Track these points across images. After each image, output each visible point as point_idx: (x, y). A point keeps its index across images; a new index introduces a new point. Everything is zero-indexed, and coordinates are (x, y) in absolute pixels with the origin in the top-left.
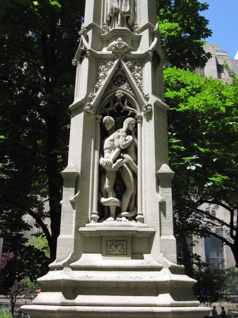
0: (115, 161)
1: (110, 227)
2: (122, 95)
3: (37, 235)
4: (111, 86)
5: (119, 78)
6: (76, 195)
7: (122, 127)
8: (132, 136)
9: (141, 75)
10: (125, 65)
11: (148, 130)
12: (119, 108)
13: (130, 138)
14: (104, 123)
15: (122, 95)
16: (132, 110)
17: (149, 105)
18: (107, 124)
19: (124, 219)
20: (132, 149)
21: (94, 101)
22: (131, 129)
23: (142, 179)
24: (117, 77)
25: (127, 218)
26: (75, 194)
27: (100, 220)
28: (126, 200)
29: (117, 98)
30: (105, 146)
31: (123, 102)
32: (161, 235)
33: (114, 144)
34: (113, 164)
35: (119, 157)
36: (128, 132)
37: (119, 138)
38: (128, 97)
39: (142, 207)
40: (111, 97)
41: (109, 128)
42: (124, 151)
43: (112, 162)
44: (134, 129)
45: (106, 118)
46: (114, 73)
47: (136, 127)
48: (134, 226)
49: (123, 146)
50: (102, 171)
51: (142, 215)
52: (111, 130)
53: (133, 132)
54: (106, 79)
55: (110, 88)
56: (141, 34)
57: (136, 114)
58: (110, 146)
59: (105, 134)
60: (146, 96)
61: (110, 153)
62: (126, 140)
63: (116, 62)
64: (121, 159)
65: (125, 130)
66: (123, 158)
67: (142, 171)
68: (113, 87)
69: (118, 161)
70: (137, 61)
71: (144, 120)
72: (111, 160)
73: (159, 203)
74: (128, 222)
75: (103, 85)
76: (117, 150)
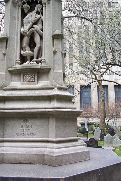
19: (35, 62)
22: (39, 10)
25: (37, 62)
35: (32, 27)
36: (38, 13)
37: (31, 17)
43: (27, 31)
44: (41, 11)
47: (42, 9)
49: (34, 21)
50: (22, 36)
51: (45, 59)
53: (40, 12)
59: (24, 15)
61: (27, 25)
66: (34, 28)
73: (53, 52)
76: (31, 23)
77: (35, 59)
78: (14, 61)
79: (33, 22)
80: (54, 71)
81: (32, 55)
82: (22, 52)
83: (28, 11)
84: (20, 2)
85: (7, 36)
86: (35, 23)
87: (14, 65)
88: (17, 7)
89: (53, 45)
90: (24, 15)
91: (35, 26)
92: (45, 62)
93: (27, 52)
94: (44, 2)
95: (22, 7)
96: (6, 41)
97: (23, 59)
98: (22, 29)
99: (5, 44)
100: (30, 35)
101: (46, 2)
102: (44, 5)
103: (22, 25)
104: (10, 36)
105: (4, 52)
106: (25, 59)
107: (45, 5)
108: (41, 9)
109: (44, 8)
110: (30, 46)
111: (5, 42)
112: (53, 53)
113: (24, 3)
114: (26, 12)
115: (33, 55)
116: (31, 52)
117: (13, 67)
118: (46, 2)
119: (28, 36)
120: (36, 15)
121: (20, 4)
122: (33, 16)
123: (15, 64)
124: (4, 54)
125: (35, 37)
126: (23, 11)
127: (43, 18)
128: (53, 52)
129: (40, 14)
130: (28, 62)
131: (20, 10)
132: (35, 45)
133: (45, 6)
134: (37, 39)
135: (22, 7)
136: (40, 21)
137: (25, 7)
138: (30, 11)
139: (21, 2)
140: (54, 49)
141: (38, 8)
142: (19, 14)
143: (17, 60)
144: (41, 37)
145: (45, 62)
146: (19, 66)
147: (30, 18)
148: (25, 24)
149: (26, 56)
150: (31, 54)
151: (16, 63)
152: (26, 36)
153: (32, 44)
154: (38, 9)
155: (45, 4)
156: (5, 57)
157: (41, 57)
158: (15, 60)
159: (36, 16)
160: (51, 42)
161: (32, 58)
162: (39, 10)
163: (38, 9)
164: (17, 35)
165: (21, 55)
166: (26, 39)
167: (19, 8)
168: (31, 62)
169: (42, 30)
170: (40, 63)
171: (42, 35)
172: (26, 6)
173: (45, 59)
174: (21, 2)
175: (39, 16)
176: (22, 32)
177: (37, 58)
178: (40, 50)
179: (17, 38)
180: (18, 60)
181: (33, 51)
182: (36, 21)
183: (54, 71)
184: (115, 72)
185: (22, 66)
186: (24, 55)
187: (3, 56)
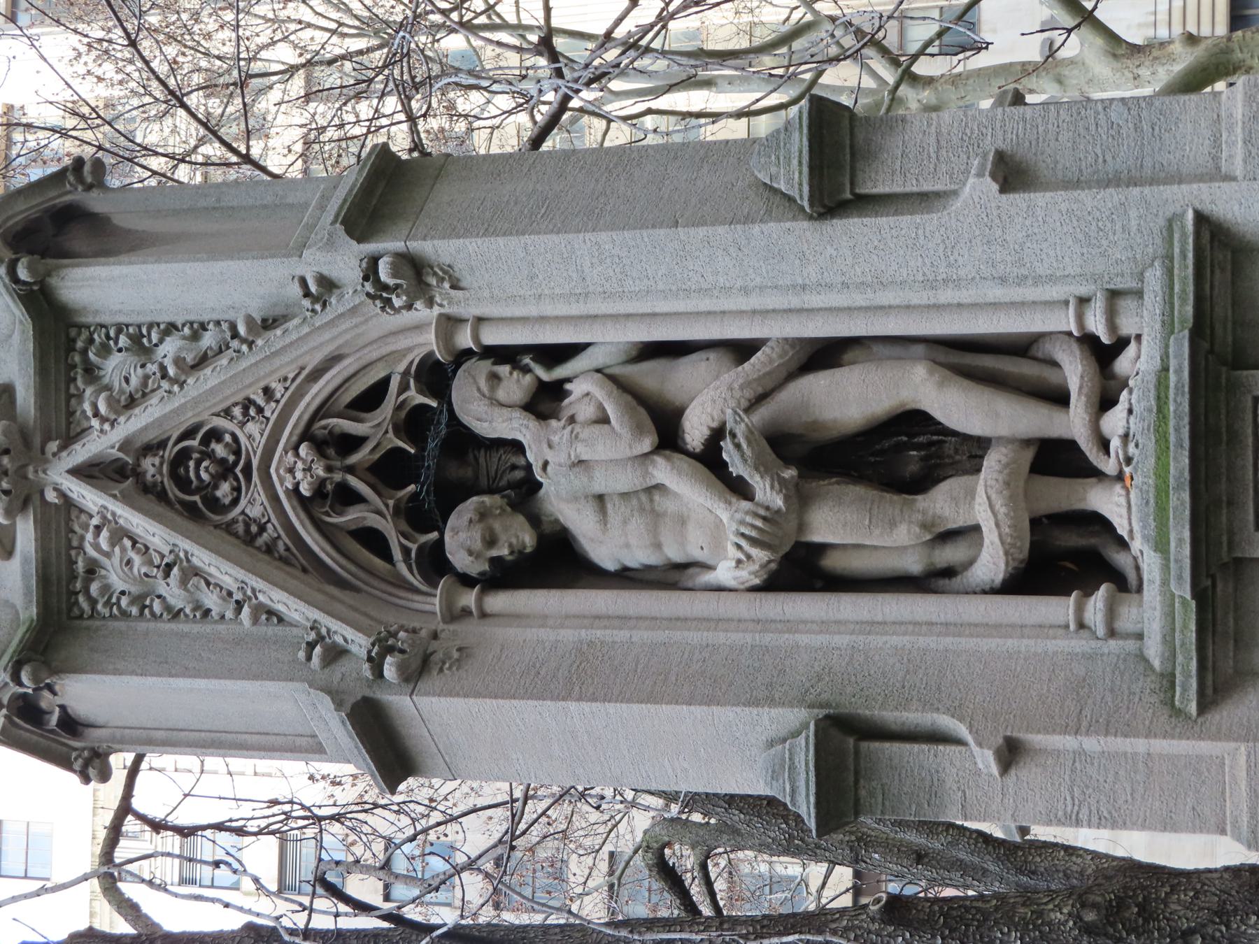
0: (739, 488)
1: (1173, 500)
2: (304, 450)
3: (153, 465)
4: (248, 521)
5: (187, 480)
6: (962, 731)
7: (517, 447)
8: (569, 380)
9: (171, 328)
10: (101, 442)
11: (532, 277)
12: (389, 470)
13: (585, 391)
14: (495, 561)
15: (304, 450)
16: (404, 387)
17: (371, 273)
18: (491, 542)
19: (1114, 422)
20: (649, 375)
21: (350, 633)
22: (515, 386)
23: (975, 306)
24: (183, 484)
25: (1106, 402)
26: (959, 742)
27: (1123, 584)
28: (958, 408)
29: (322, 483)
30: (639, 556)
31: (350, 443)
32: (1217, 175)
33: (625, 496)
34: (759, 496)
35: (710, 459)
36: (545, 402)
37: (585, 468)
38: (321, 411)
39: (606, 316)
40: (320, 526)
41: (519, 536)
42: (665, 427)
43: (745, 505)
44: (526, 370)
45: (460, 559)
46: (160, 509)
47: (506, 355)
48: (1153, 354)
49: (638, 430)
50: (800, 569)
51: (1083, 301)
52: (535, 520)
53: (544, 376)
54: (202, 558)
55: (262, 528)
56: (121, 455)
57: (430, 354)
58: (637, 525)
59: (556, 561)
60: (307, 294)
61: (682, 521)
62: (604, 420)
63: (89, 497)
64: (727, 444)
65: (532, 423)
66: (717, 434)
67: (800, 311)
68: (255, 512)
69: (737, 467)
70: (77, 358)
71: (448, 302)
72: (728, 516)
73: (1003, 190)
74: (1135, 400)
75: (241, 574)
76: (664, 471)
77: (1073, 423)
78: (1090, 657)
79: (647, 444)
80: (1230, 178)
81: (1029, 455)
82: (991, 563)
83: (521, 519)
84: (419, 602)
85: (795, 734)
86: (665, 427)
87: (1142, 658)
88: (469, 630)
89: (924, 200)
90: (556, 561)
91: (695, 431)
92: (1114, 295)
93: (984, 506)
94: (429, 342)
95: (467, 581)
96: (851, 741)
97: (1065, 557)
98: (725, 573)
99: (875, 745)
100: (790, 473)
101: (436, 310)
102: (465, 340)
103: (671, 576)
104: (801, 702)
105: (986, 760)
106: (1072, 540)
107: (460, 321)
108: (504, 370)
109: (493, 337)
110: (920, 484)
111: (864, 745)
112: (1018, 199)
113: (434, 563)
114: (528, 539)
115: (1027, 442)
116: (993, 462)
117: (1170, 655)
118: (436, 310)
119: (800, 499)
120: (572, 420)
121: (437, 601)
122: (584, 452)
123: (1131, 645)
124: (1011, 753)
125: (815, 425)
126: (505, 575)
127: (610, 341)
128: (1003, 190)
129: (560, 372)
130: (1108, 502)
131: (499, 601)
132: (913, 421)
133: (480, 320)
134: (847, 400)
135: (467, 581)
136: (649, 375)
137: (478, 545)
138: (525, 492)
139: (417, 591)
140: (979, 188)
141: (488, 409)
142: (546, 616)
143: (1081, 625)
144: (824, 355)
145: (1114, 295)
146: (1152, 593)
147: (599, 487)
148: (658, 546)
149: (1035, 522)
150: (1010, 468)
151: (1112, 633)
152: (802, 527)
153: (901, 454)
154: (501, 394)
155: (449, 323)
156: (1043, 751)
157: (1055, 364)
158: (1080, 644)
159: (586, 411)
160: (883, 221)
161: (1056, 459)
162: (515, 386)
163: (501, 394)
164: (791, 626)
165: (1023, 581)
166: (842, 522)
167: (484, 615)
168: (1109, 466)
169: (742, 350)
170: (1123, 364)
171: (801, 340)
172: (462, 540)
173: (1083, 301)
174: (417, 591)
175: (577, 389)
176: (748, 576)
177: (1060, 398)
178: (967, 357)
179: (825, 626)
180: (1080, 610)
181: (973, 450)
182: (642, 412)
183: (1230, 178)
184: (308, 805)
185: (1161, 545)
186: (1024, 554)
187: (1025, 773)
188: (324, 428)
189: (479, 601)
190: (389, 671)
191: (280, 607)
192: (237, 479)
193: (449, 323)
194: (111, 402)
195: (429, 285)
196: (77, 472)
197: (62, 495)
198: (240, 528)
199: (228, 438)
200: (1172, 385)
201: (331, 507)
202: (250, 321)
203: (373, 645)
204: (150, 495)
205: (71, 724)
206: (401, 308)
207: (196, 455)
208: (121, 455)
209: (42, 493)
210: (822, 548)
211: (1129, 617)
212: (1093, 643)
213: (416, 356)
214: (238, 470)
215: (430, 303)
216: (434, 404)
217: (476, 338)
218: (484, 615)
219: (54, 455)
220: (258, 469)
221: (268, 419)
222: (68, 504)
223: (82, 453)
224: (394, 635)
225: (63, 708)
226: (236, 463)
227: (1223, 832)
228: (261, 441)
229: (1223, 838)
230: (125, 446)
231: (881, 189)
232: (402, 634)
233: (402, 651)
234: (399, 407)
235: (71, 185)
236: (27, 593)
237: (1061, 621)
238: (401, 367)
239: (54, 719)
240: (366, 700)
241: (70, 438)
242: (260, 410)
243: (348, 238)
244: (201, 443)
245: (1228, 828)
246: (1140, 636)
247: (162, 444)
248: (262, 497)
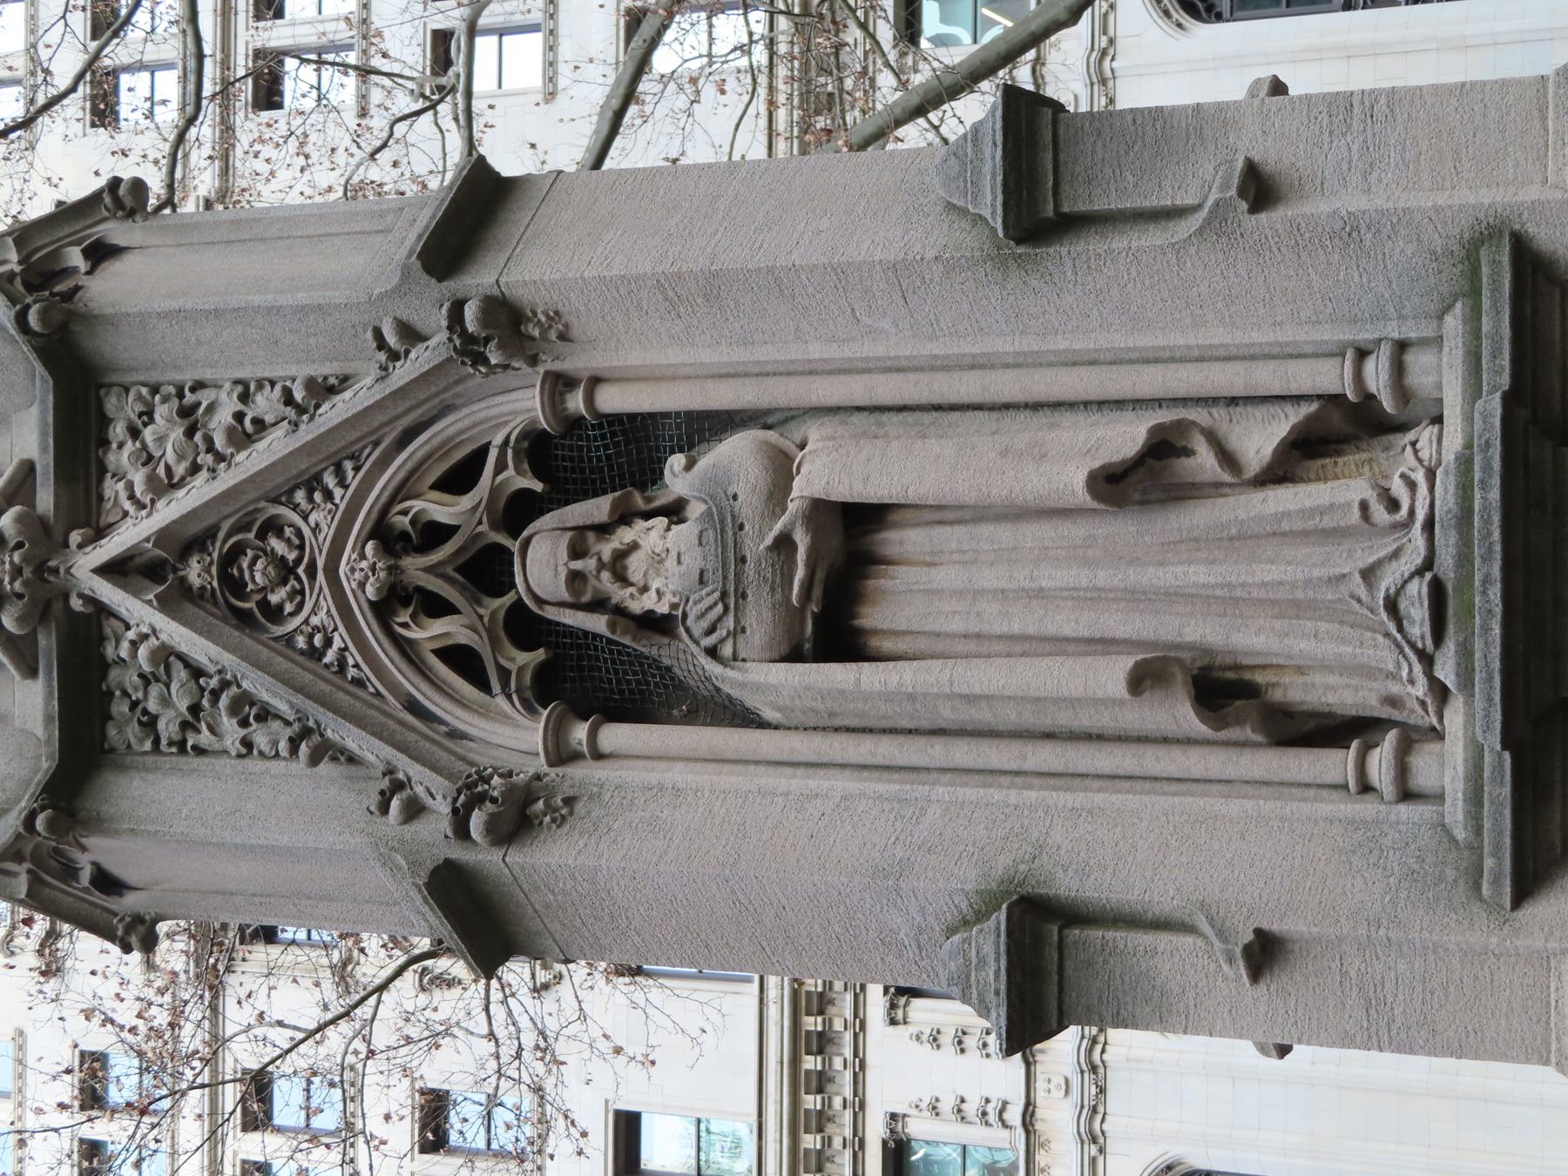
16: (500, 467)
31: (434, 534)
38: (402, 491)
55: (328, 642)
56: (159, 552)
99: (1096, 934)
101: (541, 370)
111: (1075, 933)
133: (595, 381)
143: (1366, 788)
151: (1407, 794)
188: (405, 513)
189: (593, 734)
190: (477, 821)
191: (351, 745)
192: (298, 579)
193: (559, 384)
194: (152, 480)
195: (533, 339)
196: (113, 570)
197: (91, 600)
198: (301, 642)
199: (288, 531)
200: (1477, 508)
201: (413, 617)
202: (311, 384)
203: (459, 792)
204: (178, 600)
205: (107, 882)
206: (496, 366)
207: (250, 553)
208: (159, 552)
209: (66, 597)
210: (875, 632)
211: (1426, 768)
212: (1383, 808)
213: (514, 427)
214: (300, 571)
215: (533, 361)
216: (538, 486)
217: (590, 400)
218: (599, 756)
219: (80, 546)
220: (324, 570)
221: (337, 506)
222: (101, 610)
223: (111, 547)
224: (487, 780)
225: (96, 865)
226: (298, 561)
227: (1546, 1063)
228: (328, 533)
229: (1547, 1068)
230: (163, 536)
231: (1100, 205)
232: (496, 780)
233: (494, 800)
234: (494, 491)
235: (107, 209)
236: (48, 719)
237: (1339, 780)
238: (498, 439)
239: (86, 876)
240: (448, 863)
241: (100, 533)
242: (329, 496)
243: (426, 277)
244: (257, 537)
245: (1553, 1060)
246: (1439, 797)
247: (211, 533)
248: (327, 603)
